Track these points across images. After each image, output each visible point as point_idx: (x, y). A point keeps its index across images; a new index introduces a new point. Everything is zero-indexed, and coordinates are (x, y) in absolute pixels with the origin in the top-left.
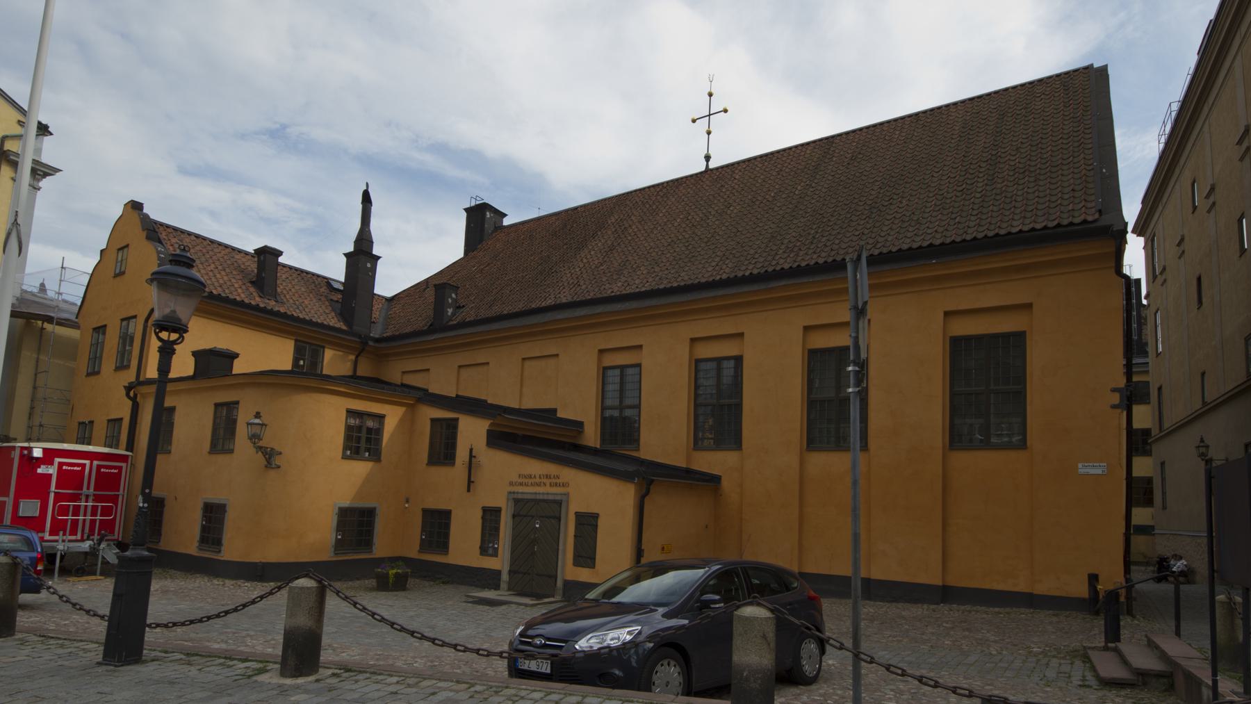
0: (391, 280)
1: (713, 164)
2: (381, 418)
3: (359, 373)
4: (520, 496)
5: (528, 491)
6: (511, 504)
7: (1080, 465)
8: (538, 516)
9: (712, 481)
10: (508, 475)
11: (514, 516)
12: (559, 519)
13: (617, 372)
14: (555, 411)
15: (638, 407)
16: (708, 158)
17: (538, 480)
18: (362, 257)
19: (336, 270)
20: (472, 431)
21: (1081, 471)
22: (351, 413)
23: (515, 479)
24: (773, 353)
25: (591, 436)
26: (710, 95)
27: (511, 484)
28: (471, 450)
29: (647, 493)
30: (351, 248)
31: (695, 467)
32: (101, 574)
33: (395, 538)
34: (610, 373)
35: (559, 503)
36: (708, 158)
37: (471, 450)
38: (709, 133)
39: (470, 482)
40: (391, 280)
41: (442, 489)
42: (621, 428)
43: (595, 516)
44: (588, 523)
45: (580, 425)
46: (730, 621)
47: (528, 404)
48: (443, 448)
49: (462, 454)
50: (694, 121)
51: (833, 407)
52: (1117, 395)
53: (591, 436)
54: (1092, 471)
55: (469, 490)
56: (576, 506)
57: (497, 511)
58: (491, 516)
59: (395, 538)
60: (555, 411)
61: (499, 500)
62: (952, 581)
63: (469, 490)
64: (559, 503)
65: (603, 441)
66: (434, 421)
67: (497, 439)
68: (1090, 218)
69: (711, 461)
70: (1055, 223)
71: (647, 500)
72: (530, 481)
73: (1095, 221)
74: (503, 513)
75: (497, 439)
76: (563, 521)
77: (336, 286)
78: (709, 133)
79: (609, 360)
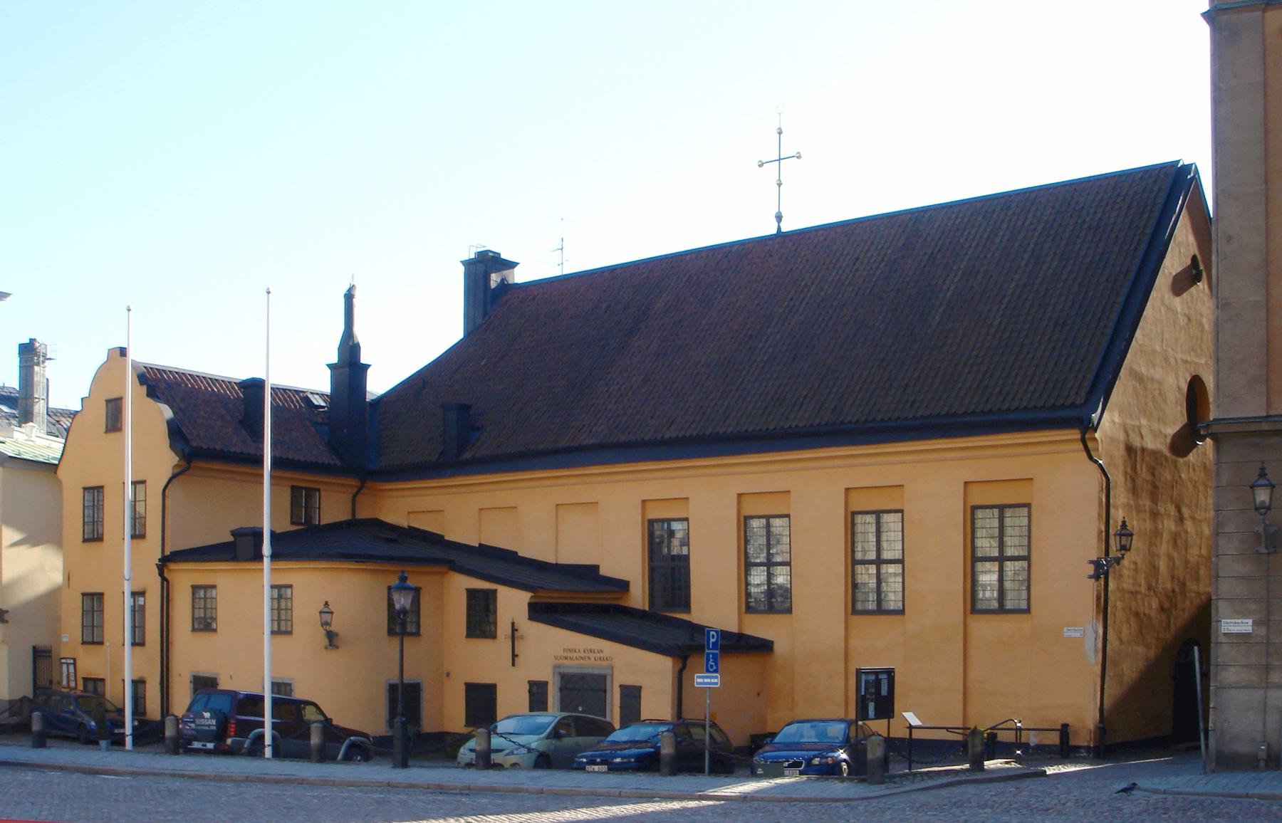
0: (378, 384)
1: (787, 227)
4: (565, 671)
6: (558, 678)
8: (582, 690)
9: (765, 647)
10: (553, 649)
11: (561, 690)
12: (605, 691)
14: (597, 567)
16: (779, 218)
17: (582, 654)
18: (350, 367)
19: (317, 382)
20: (512, 603)
21: (1067, 634)
23: (560, 653)
25: (638, 597)
26: (780, 133)
27: (556, 658)
28: (513, 624)
29: (684, 667)
32: (279, 753)
33: (448, 712)
35: (604, 678)
36: (779, 218)
37: (513, 624)
38: (780, 185)
39: (514, 656)
40: (378, 384)
41: (484, 661)
42: (670, 574)
43: (639, 689)
44: (632, 695)
45: (624, 586)
47: (567, 558)
48: (481, 618)
49: (503, 628)
52: (1092, 567)
53: (638, 597)
56: (622, 677)
57: (545, 684)
60: (597, 567)
63: (513, 664)
64: (604, 678)
65: (652, 604)
66: (472, 593)
67: (539, 612)
69: (759, 627)
71: (685, 672)
72: (575, 655)
74: (550, 687)
75: (539, 612)
78: (780, 185)
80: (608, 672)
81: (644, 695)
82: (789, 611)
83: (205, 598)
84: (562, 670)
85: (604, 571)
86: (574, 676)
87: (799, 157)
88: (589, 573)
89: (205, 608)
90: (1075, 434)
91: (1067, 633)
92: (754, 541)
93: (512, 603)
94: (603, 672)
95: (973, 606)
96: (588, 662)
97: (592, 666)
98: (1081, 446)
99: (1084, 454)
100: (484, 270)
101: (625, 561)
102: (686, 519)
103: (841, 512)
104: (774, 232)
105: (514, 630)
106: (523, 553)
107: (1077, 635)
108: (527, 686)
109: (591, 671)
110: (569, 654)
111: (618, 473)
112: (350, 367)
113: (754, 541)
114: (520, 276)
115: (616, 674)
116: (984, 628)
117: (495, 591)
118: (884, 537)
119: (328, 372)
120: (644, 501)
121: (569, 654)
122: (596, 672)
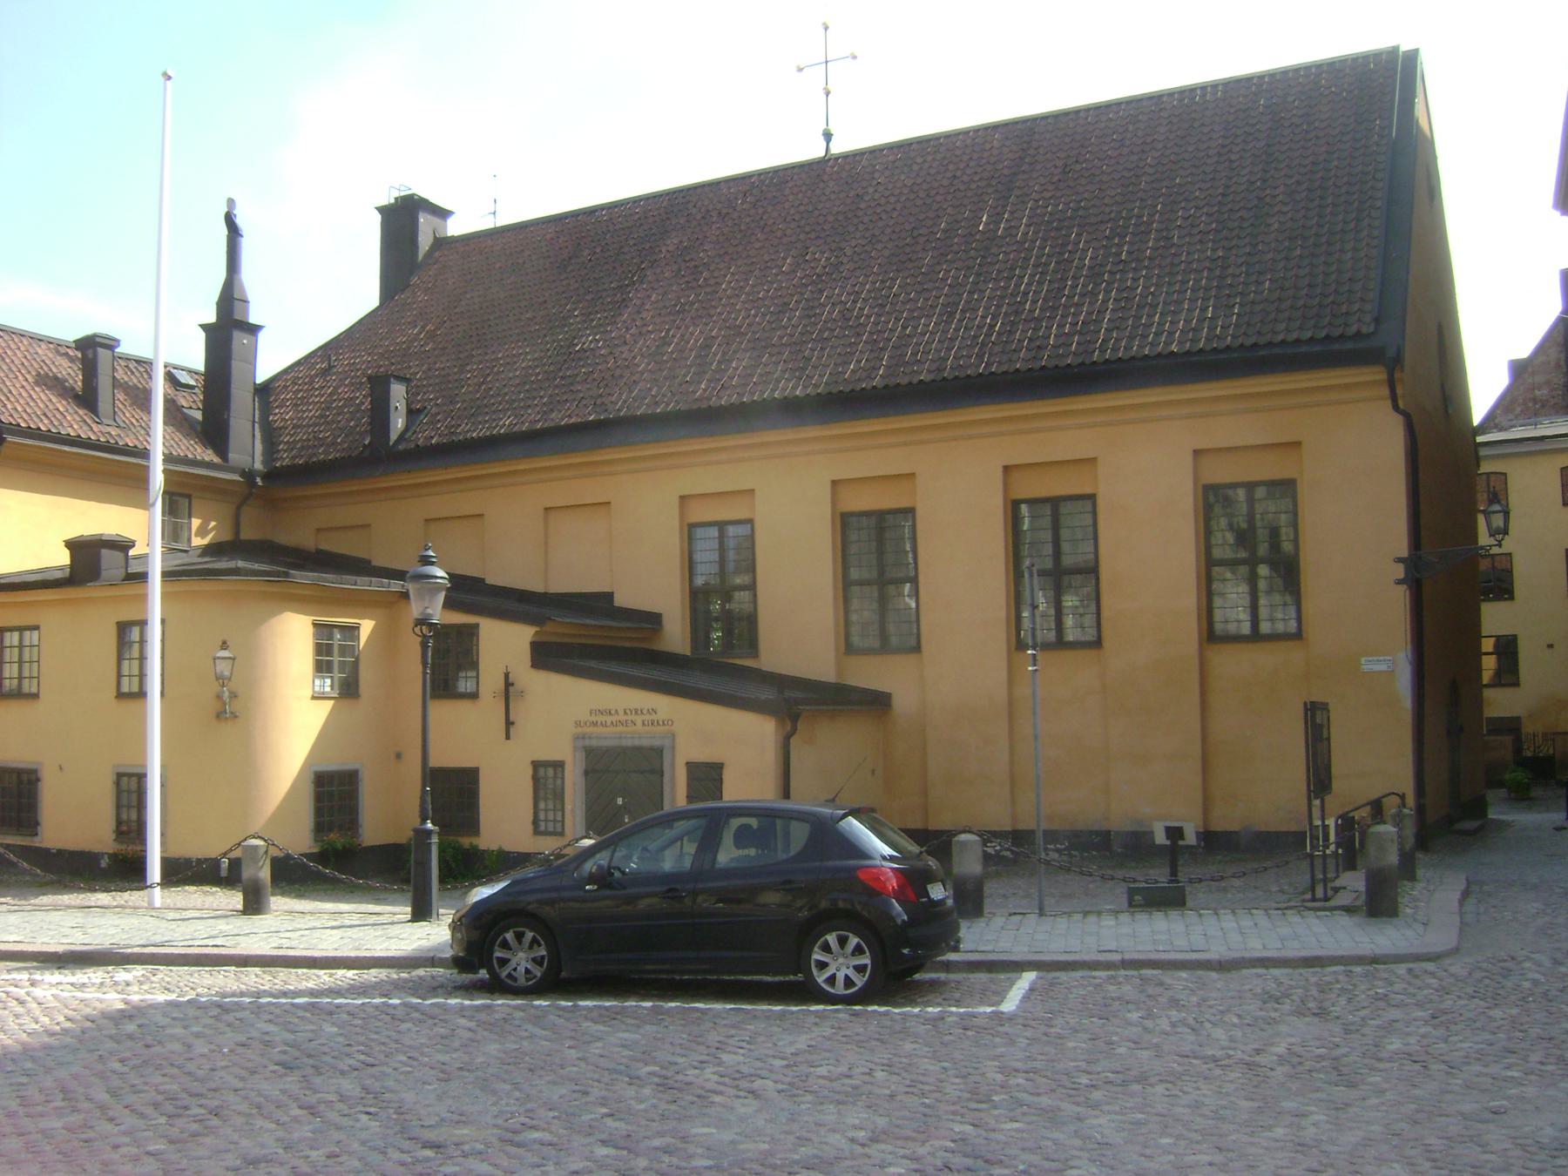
1: (837, 148)
2: (356, 628)
3: (244, 536)
4: (594, 743)
5: (607, 735)
6: (581, 755)
7: (1363, 660)
9: (877, 702)
11: (586, 773)
13: (714, 532)
15: (752, 587)
16: (828, 136)
17: (622, 717)
18: (229, 328)
20: (504, 644)
21: (1365, 668)
22: (315, 625)
24: (956, 482)
27: (578, 724)
28: (507, 676)
29: (794, 731)
30: (211, 317)
31: (853, 681)
34: (699, 532)
36: (828, 136)
37: (507, 676)
38: (828, 94)
39: (509, 723)
40: (273, 356)
44: (707, 777)
45: (652, 621)
46: (950, 842)
50: (800, 70)
51: (1052, 551)
52: (1401, 567)
53: (676, 636)
54: (1377, 668)
55: (508, 737)
57: (558, 766)
58: (545, 775)
59: (389, 812)
61: (561, 749)
62: (1227, 819)
63: (508, 737)
64: (659, 752)
67: (545, 656)
68: (1365, 330)
69: (869, 674)
70: (1323, 334)
72: (609, 719)
73: (1368, 336)
75: (545, 656)
76: (666, 779)
77: (184, 378)
79: (700, 513)
80: (667, 742)
81: (727, 776)
82: (917, 649)
83: (21, 646)
84: (587, 743)
85: (619, 601)
86: (608, 751)
87: (855, 57)
88: (598, 604)
89: (21, 662)
90: (1376, 374)
91: (1370, 665)
92: (876, 548)
93: (504, 644)
94: (657, 743)
95: (1211, 636)
96: (631, 728)
97: (638, 733)
98: (1386, 391)
99: (1389, 402)
100: (403, 219)
101: (652, 582)
102: (750, 521)
103: (998, 501)
104: (822, 154)
105: (508, 684)
106: (490, 581)
107: (1383, 667)
108: (530, 771)
109: (637, 743)
110: (600, 718)
111: (644, 458)
112: (229, 328)
113: (876, 548)
114: (456, 227)
115: (681, 743)
116: (1231, 663)
117: (477, 626)
118: (1065, 534)
119: (202, 335)
120: (682, 498)
121: (600, 718)
122: (645, 743)
